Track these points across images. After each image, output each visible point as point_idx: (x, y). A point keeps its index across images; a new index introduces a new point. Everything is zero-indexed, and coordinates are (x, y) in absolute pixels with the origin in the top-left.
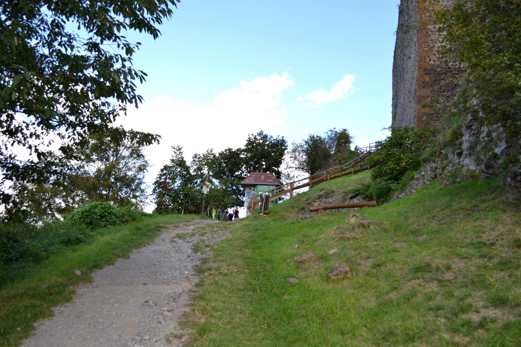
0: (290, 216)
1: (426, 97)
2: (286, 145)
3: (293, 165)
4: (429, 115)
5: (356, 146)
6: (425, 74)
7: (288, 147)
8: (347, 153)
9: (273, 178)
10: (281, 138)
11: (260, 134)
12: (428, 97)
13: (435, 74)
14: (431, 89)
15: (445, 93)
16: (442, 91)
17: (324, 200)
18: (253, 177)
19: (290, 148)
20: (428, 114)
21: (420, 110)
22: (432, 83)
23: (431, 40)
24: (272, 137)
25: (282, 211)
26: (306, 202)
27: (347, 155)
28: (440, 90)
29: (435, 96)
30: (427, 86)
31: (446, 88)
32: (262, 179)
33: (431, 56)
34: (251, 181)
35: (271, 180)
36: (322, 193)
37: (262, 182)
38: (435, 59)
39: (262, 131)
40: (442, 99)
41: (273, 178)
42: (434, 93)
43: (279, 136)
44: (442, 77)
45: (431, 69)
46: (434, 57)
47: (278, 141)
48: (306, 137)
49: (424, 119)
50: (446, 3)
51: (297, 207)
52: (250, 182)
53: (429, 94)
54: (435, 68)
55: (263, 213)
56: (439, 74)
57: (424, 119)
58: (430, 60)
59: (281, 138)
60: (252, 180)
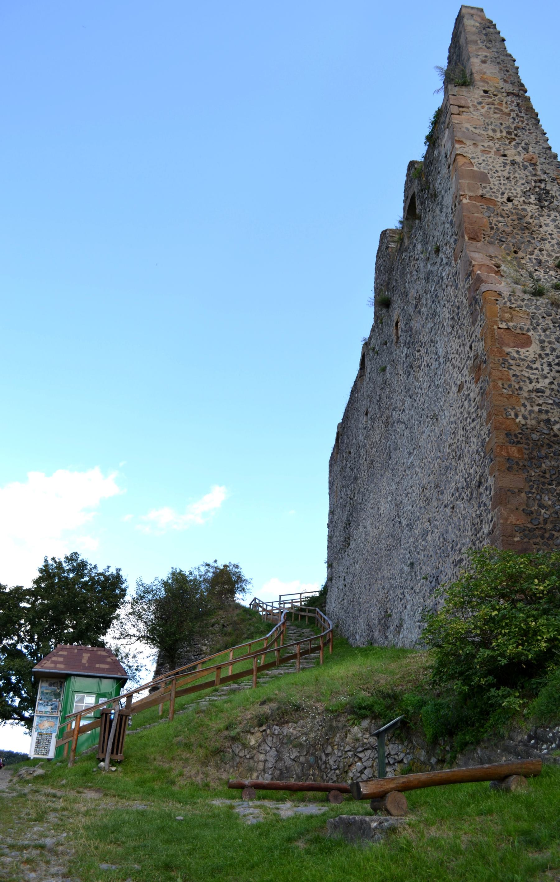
0: (186, 770)
1: (517, 491)
2: (123, 586)
3: (133, 631)
4: (527, 532)
5: (255, 599)
6: (510, 442)
7: (128, 592)
8: (238, 612)
9: (109, 660)
10: (115, 572)
11: (72, 559)
12: (520, 491)
13: (528, 444)
14: (525, 476)
15: (554, 486)
16: (546, 481)
17: (276, 729)
18: (61, 656)
19: (131, 593)
20: (524, 530)
21: (507, 519)
22: (526, 463)
23: (514, 375)
24: (95, 567)
25: (158, 757)
26: (226, 733)
27: (238, 615)
28: (543, 480)
29: (534, 490)
30: (515, 467)
31: (554, 477)
32: (84, 661)
33: (517, 408)
34: (59, 666)
35: (106, 666)
36: (266, 709)
37: (84, 668)
38: (526, 413)
39: (76, 553)
40: (549, 499)
41: (109, 660)
42: (531, 483)
43: (108, 567)
44: (543, 452)
45: (519, 433)
46: (523, 409)
47: (107, 578)
48: (165, 575)
49: (516, 539)
50: (535, 311)
51: (201, 747)
52: (55, 668)
53: (521, 485)
54: (528, 431)
55: (107, 760)
56: (538, 446)
57: (516, 539)
58: (517, 416)
59: (115, 572)
60: (60, 663)
